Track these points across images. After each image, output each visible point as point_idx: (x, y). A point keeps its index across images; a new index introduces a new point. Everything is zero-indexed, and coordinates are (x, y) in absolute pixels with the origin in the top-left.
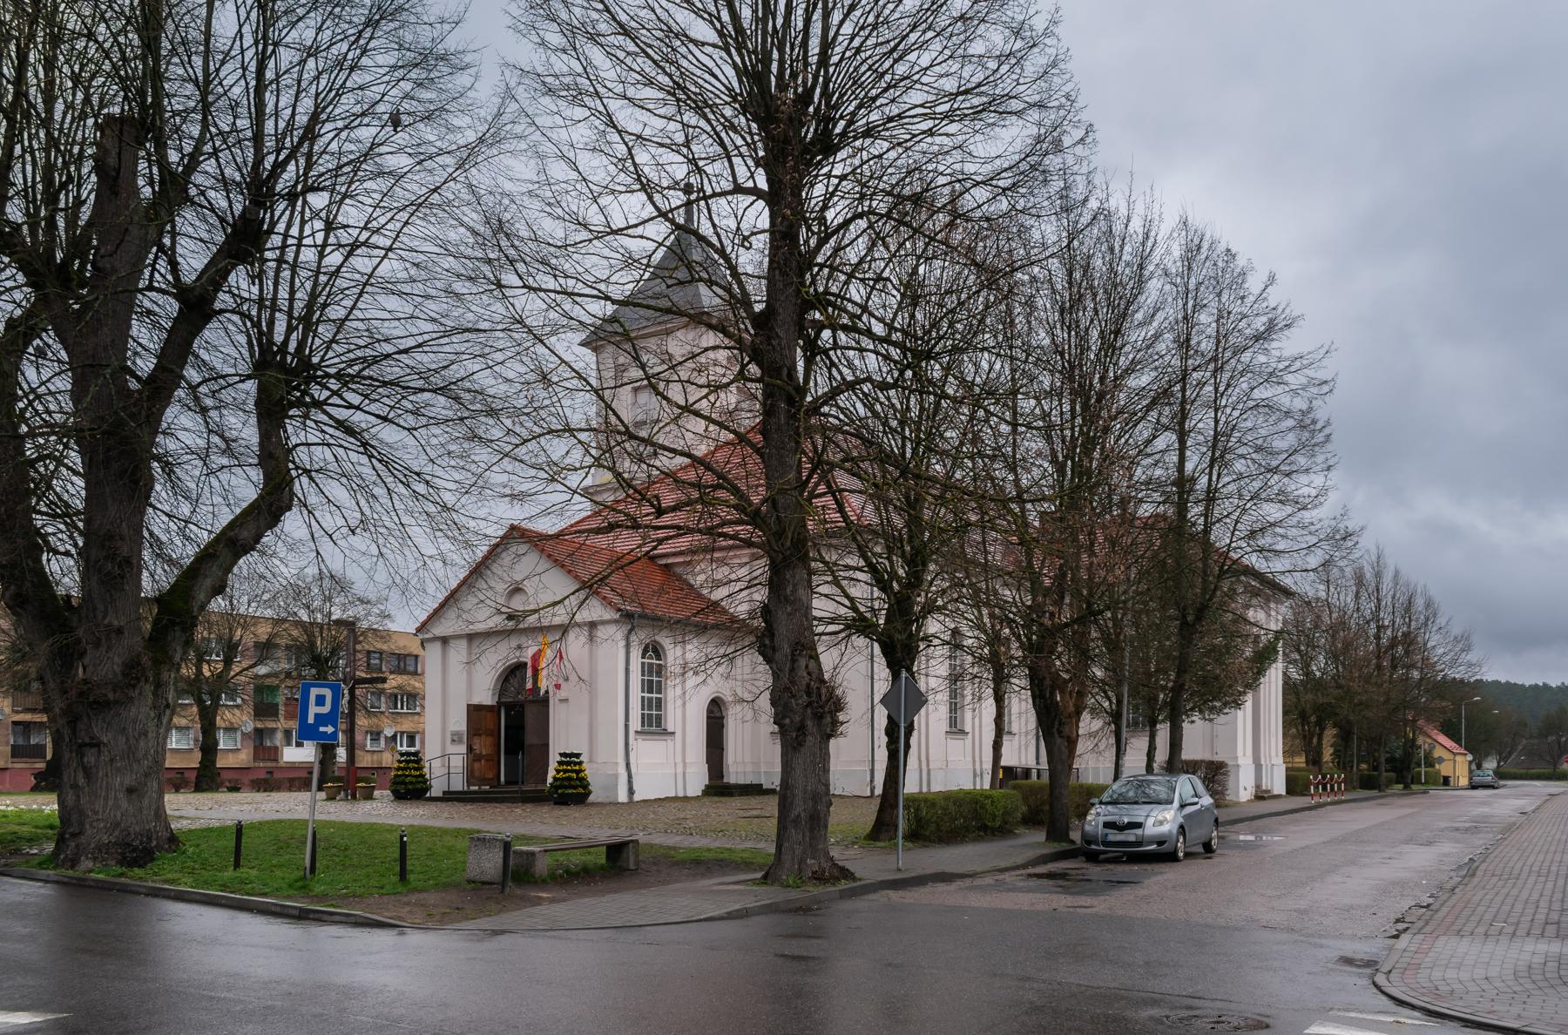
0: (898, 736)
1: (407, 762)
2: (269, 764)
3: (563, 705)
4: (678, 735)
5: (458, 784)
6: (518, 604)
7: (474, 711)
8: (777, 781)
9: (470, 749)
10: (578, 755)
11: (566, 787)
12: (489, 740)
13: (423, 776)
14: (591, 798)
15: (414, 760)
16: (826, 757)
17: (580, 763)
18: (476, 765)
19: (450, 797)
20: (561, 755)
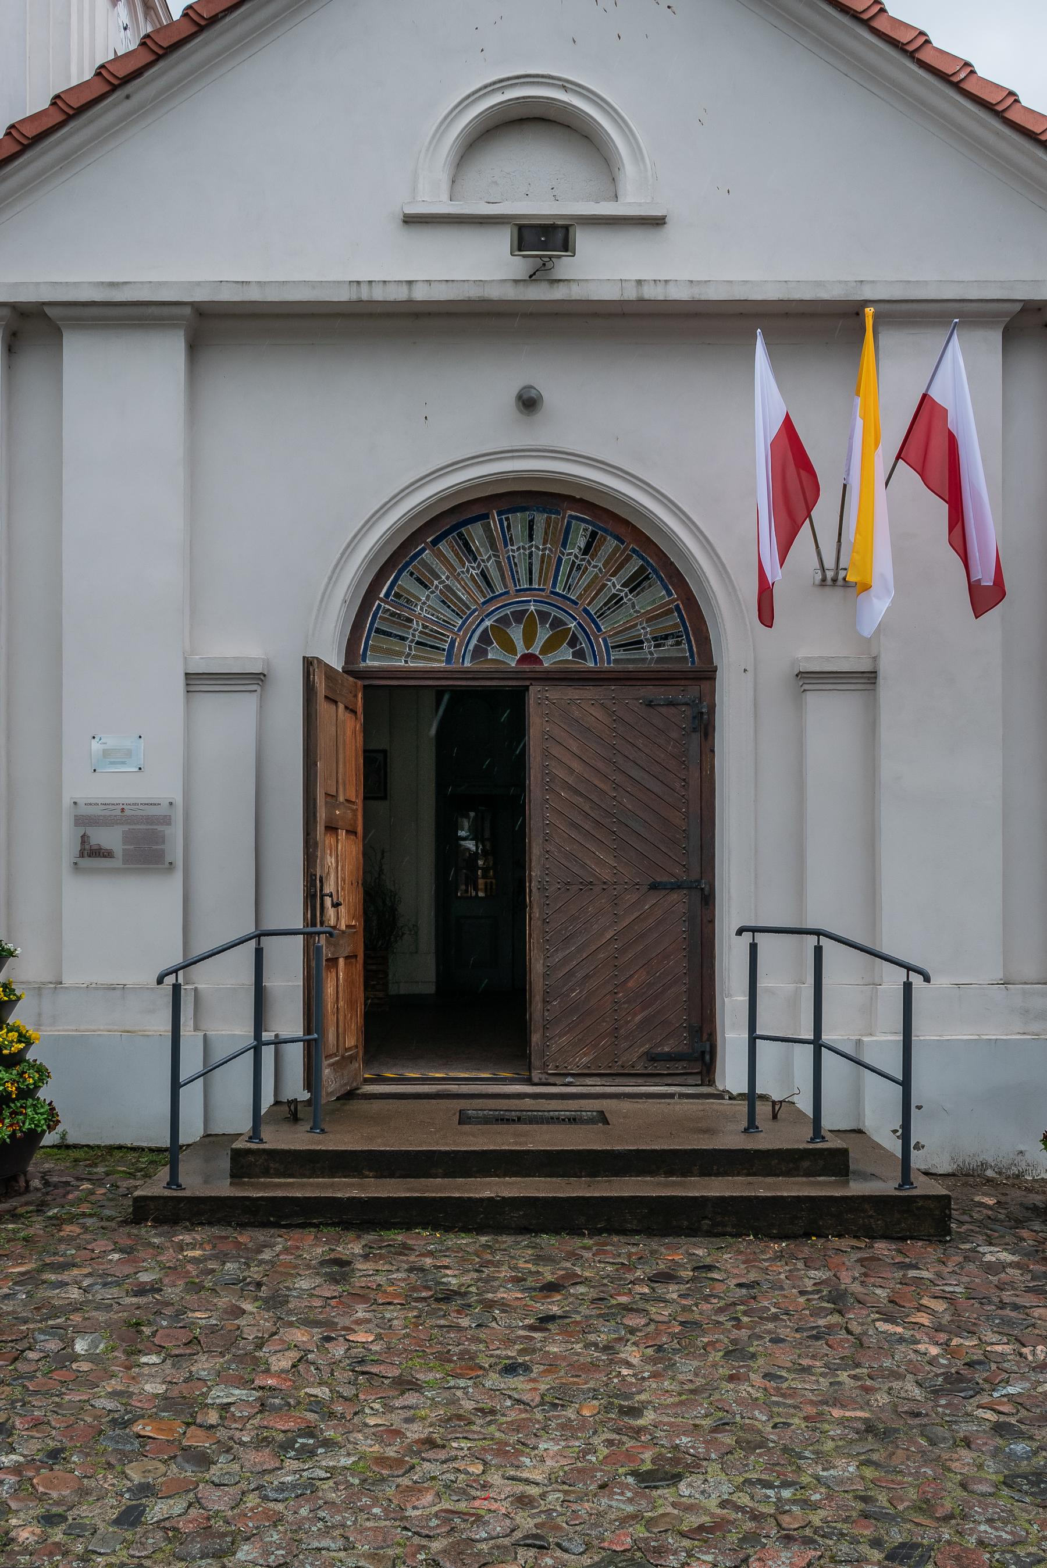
3: (830, 715)
19: (260, 1194)
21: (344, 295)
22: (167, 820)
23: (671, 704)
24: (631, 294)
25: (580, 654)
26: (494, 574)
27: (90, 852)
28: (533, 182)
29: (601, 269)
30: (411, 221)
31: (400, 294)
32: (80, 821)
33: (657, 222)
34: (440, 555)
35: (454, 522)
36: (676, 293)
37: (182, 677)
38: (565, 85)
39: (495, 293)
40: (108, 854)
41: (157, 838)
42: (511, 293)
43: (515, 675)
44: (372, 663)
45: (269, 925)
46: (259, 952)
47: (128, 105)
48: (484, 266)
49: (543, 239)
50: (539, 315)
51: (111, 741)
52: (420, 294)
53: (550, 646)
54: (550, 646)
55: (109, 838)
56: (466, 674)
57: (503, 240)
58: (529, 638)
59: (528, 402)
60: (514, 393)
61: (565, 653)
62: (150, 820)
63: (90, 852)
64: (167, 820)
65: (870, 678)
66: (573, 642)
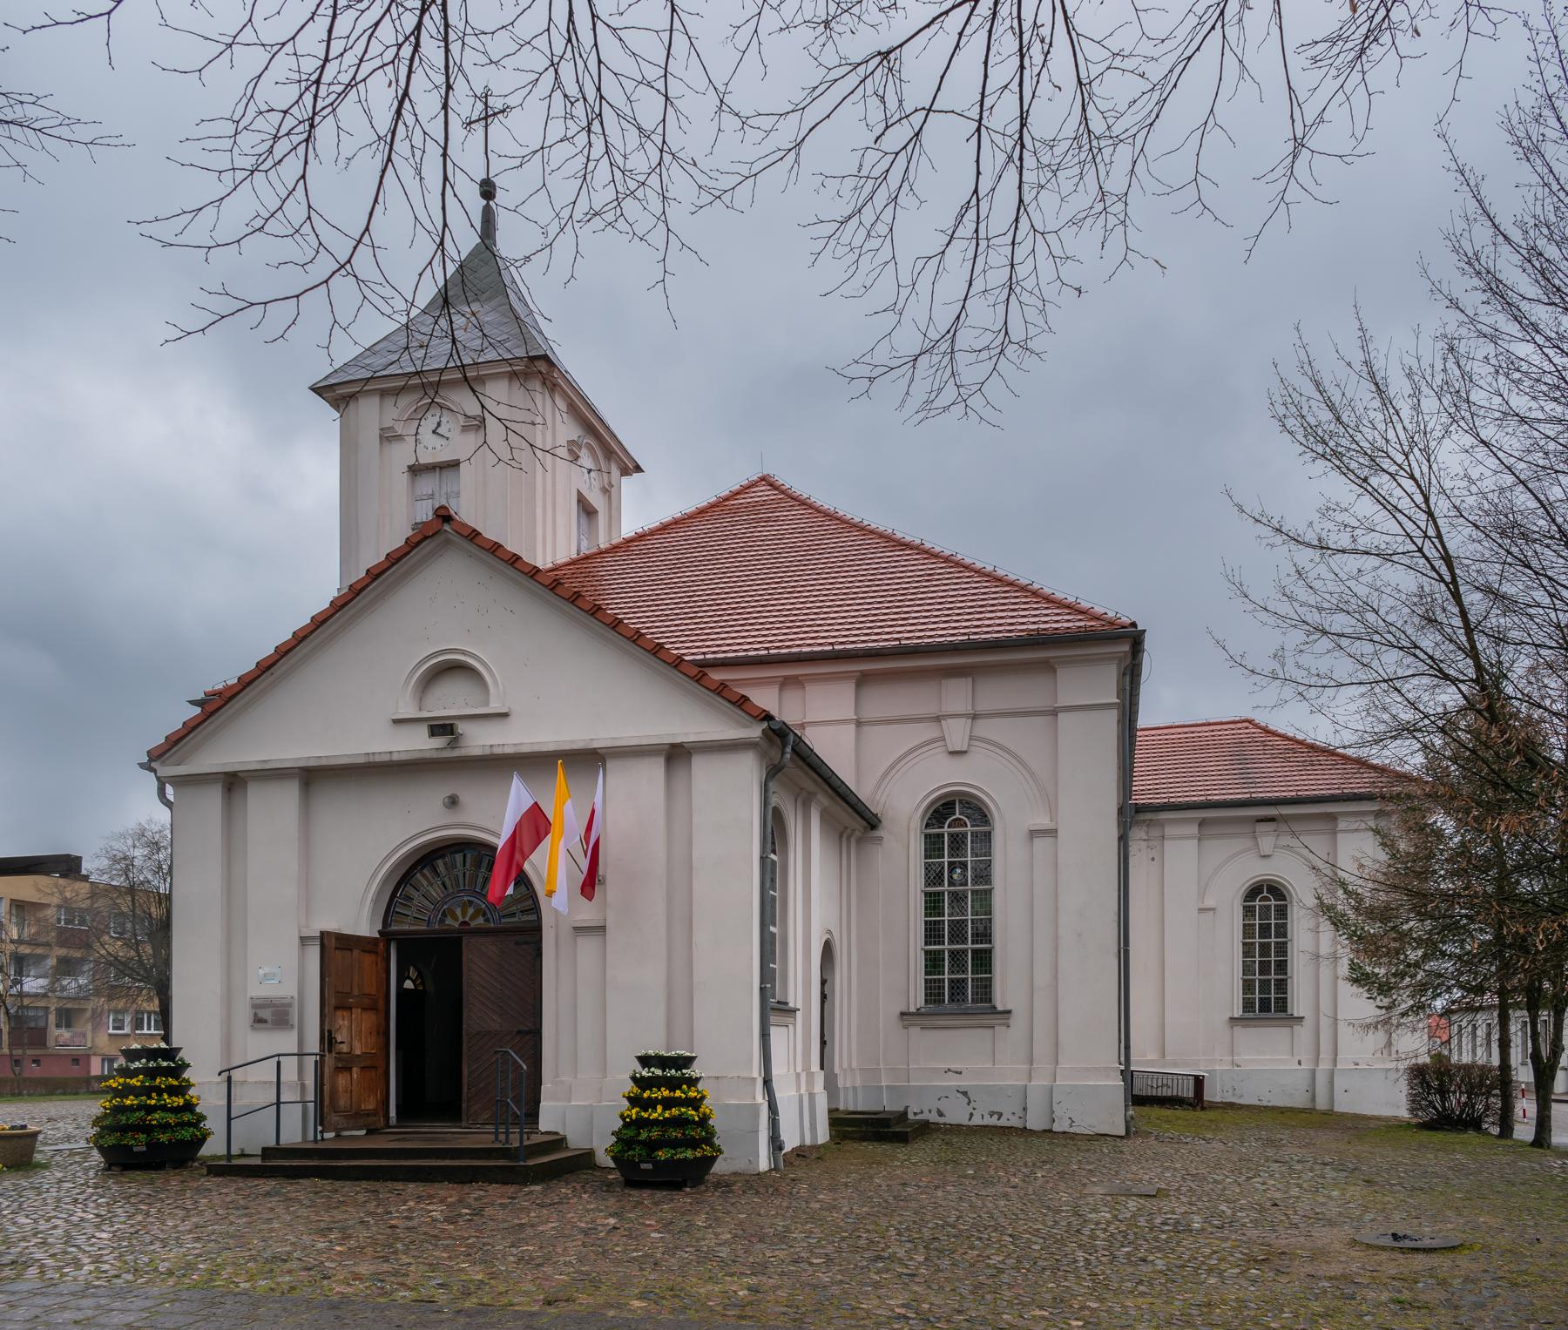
0: (1460, 1054)
1: (151, 1073)
2: (38, 1052)
3: (587, 945)
4: (1018, 1021)
5: (293, 1132)
6: (450, 700)
7: (335, 948)
8: (1191, 1094)
9: (328, 1040)
10: (688, 1061)
11: (674, 1144)
12: (368, 1020)
13: (189, 1107)
14: (719, 1167)
15: (165, 1065)
16: (1343, 1114)
17: (693, 1082)
18: (342, 1080)
19: (280, 1165)
20: (645, 1061)
21: (362, 760)
22: (290, 1005)
23: (527, 943)
24: (487, 751)
25: (487, 920)
26: (448, 883)
27: (258, 1021)
28: (450, 700)
29: (480, 740)
30: (396, 722)
31: (386, 758)
32: (255, 1006)
33: (505, 715)
34: (424, 876)
35: (426, 859)
36: (508, 750)
37: (296, 941)
38: (464, 653)
39: (427, 755)
40: (265, 1021)
41: (287, 1013)
42: (435, 755)
43: (459, 931)
44: (394, 928)
45: (306, 1051)
46: (279, 1063)
47: (272, 678)
48: (419, 743)
49: (442, 728)
50: (449, 762)
51: (267, 970)
52: (395, 757)
53: (473, 917)
54: (473, 917)
55: (265, 1014)
56: (434, 932)
57: (423, 730)
58: (464, 914)
59: (453, 802)
60: (440, 803)
61: (480, 920)
62: (283, 1005)
63: (258, 1021)
64: (290, 1005)
65: (603, 928)
66: (484, 914)
